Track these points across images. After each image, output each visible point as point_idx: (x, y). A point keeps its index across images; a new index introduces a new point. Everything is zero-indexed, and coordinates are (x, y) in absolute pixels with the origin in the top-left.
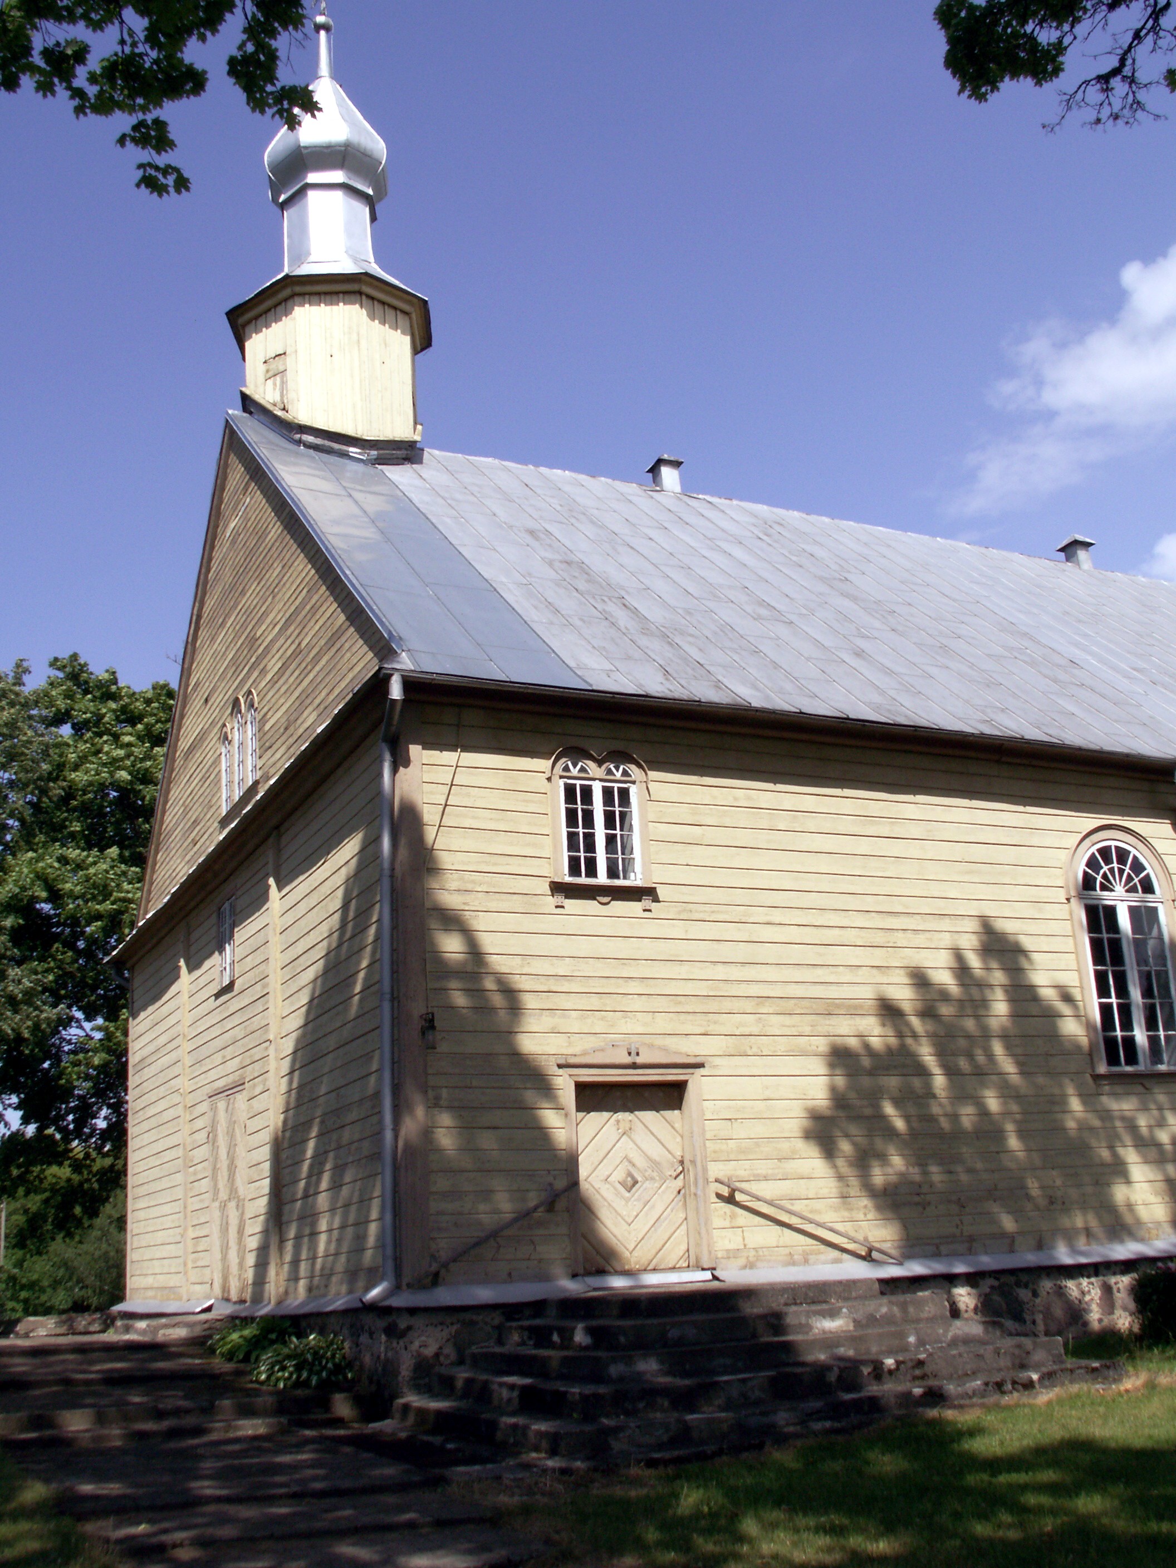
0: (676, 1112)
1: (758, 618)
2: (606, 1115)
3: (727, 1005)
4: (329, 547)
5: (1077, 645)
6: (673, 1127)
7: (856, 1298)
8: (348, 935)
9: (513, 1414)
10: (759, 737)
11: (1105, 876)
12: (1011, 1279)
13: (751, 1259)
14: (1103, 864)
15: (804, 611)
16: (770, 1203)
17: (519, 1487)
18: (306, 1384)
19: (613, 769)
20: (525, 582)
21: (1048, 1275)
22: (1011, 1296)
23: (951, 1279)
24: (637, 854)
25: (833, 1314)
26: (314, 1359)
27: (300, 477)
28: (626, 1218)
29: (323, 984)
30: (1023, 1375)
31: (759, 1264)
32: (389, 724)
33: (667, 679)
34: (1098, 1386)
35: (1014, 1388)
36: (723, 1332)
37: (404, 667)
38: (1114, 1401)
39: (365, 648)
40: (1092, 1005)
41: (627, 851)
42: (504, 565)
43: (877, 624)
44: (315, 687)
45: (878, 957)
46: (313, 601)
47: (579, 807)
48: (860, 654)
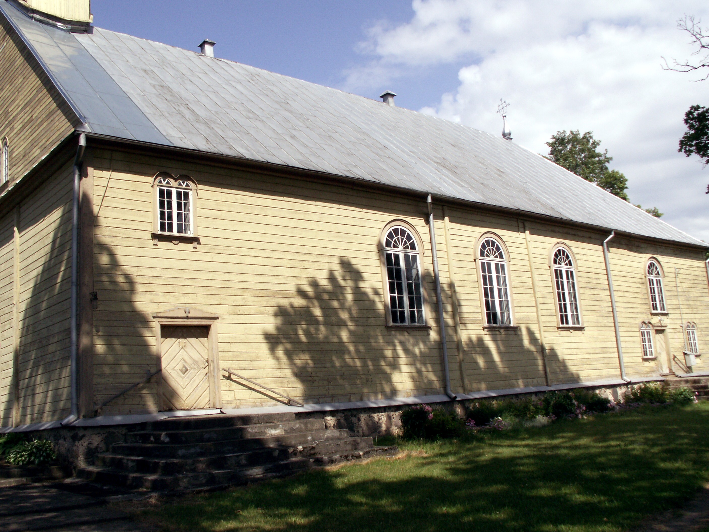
0: (205, 339)
1: (248, 118)
2: (174, 340)
3: (230, 291)
4: (49, 70)
5: (387, 139)
6: (204, 346)
7: (285, 421)
8: (54, 255)
9: (134, 472)
10: (249, 172)
11: (395, 241)
12: (349, 413)
13: (238, 404)
14: (394, 236)
15: (269, 116)
16: (247, 380)
17: (140, 504)
18: (33, 462)
19: (182, 183)
20: (142, 94)
21: (365, 412)
22: (348, 419)
23: (324, 413)
24: (191, 222)
25: (275, 427)
26: (37, 451)
27: (33, 35)
28: (182, 386)
29: (41, 277)
30: (356, 453)
31: (241, 407)
32: (79, 157)
33: (208, 143)
34: (387, 457)
35: (352, 458)
36: (225, 436)
37: (86, 131)
38: (394, 463)
39: (66, 120)
40: (387, 296)
41: (186, 221)
42: (132, 85)
43: (301, 124)
44: (39, 137)
45: (296, 272)
46: (39, 96)
47: (166, 199)
48: (293, 137)
